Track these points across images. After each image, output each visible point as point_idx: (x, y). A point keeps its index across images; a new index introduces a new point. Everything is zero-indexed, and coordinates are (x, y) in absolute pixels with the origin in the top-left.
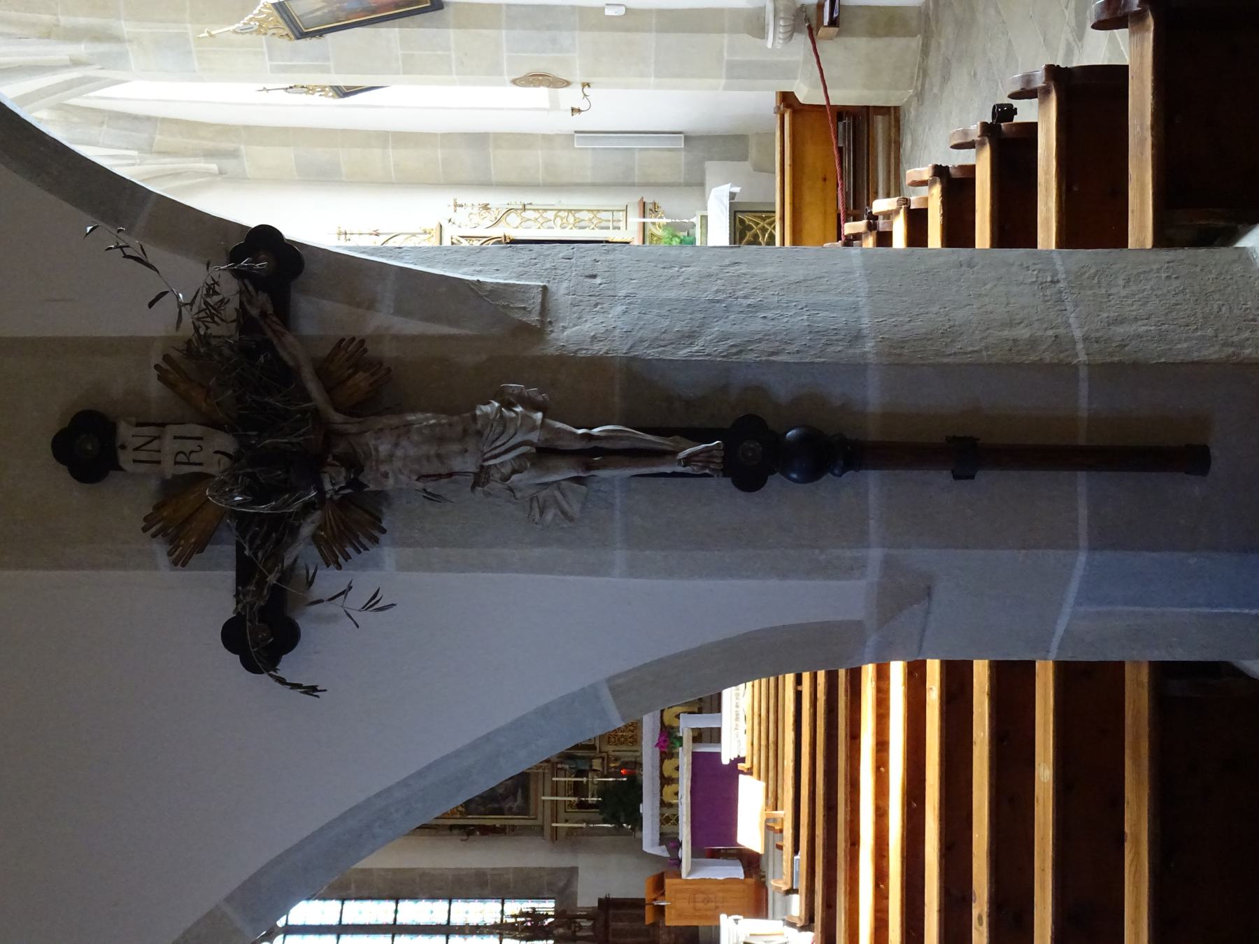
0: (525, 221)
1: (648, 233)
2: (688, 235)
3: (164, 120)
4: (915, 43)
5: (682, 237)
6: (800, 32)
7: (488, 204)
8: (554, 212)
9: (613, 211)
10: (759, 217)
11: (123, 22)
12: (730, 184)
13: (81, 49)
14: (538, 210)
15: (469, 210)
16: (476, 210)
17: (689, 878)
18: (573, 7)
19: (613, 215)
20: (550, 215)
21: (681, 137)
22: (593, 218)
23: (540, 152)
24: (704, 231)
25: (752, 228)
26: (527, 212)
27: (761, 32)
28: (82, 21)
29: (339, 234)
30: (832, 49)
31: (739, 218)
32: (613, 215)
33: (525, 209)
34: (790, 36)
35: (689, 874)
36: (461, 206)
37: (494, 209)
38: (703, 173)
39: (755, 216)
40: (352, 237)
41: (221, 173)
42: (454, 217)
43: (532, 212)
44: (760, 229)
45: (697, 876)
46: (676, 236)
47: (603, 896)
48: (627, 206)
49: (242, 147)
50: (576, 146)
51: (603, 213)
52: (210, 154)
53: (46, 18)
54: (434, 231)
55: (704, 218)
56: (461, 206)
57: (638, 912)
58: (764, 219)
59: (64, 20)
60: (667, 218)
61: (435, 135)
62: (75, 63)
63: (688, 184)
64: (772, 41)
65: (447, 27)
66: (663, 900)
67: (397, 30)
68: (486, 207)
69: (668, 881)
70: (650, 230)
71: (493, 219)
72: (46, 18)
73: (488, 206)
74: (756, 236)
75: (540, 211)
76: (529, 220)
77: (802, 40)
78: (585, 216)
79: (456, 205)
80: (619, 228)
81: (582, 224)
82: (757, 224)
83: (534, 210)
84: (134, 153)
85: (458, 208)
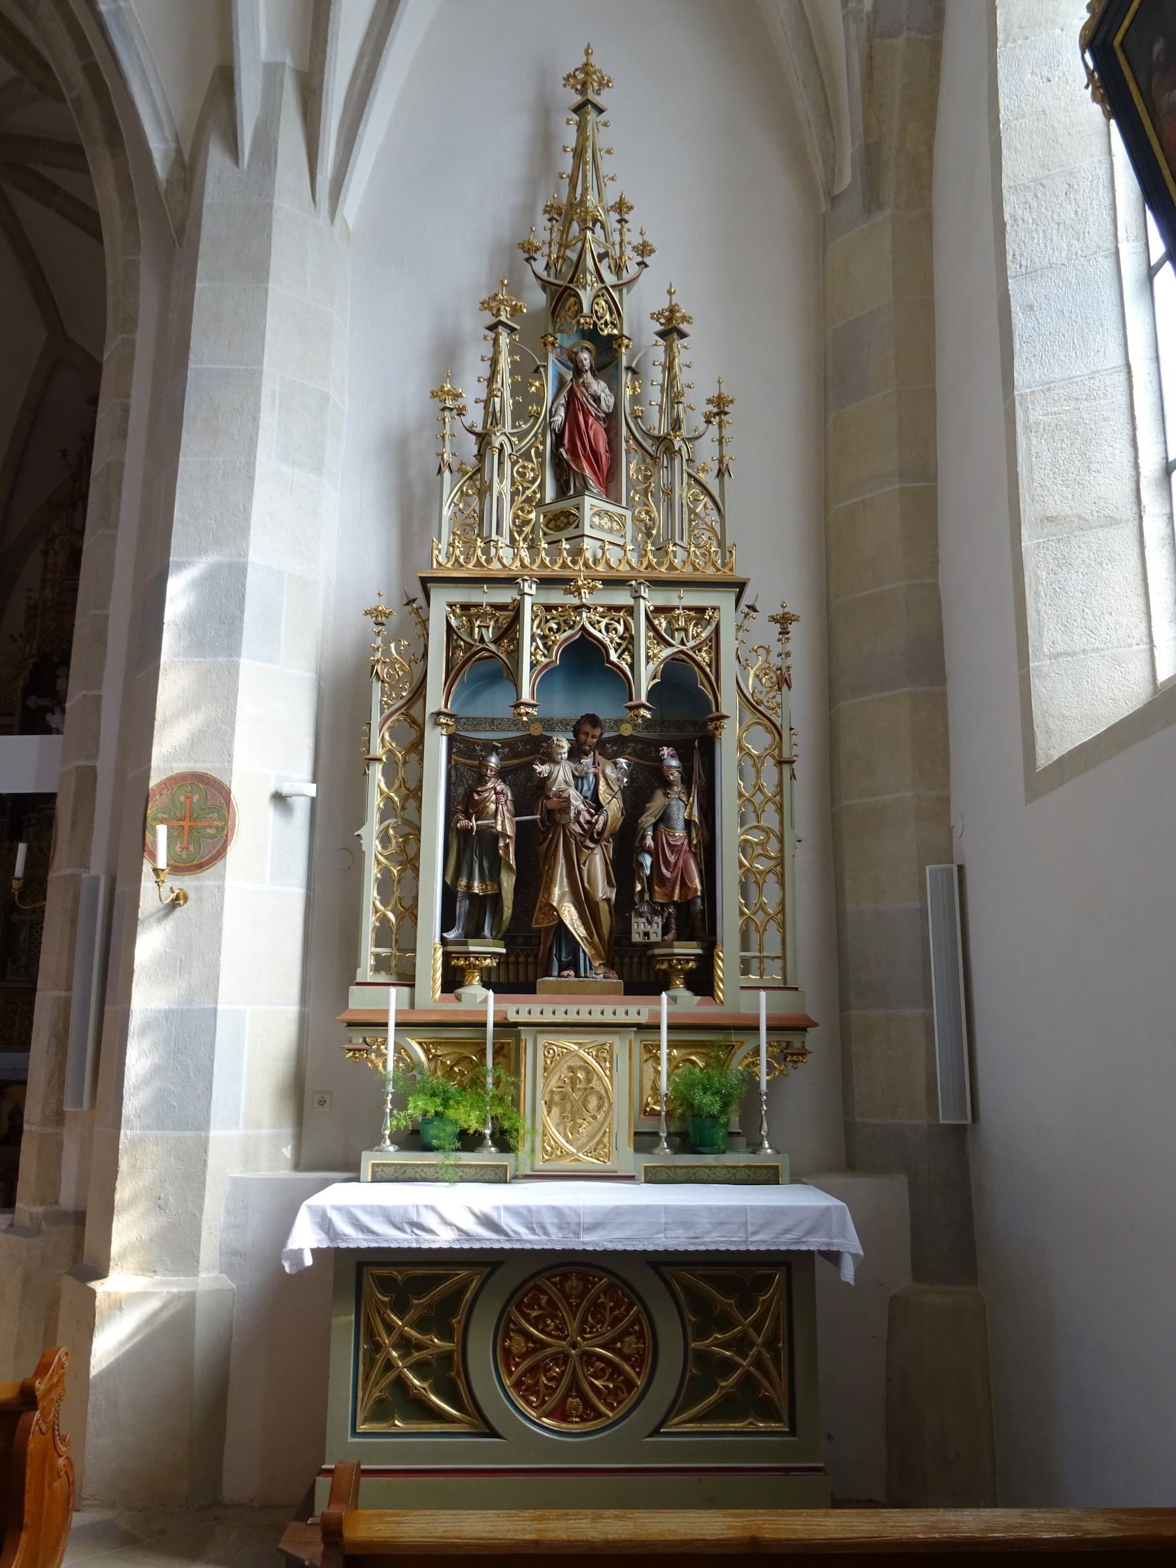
0: (755, 765)
1: (734, 1038)
2: (731, 1134)
3: (936, 48)
5: (723, 1120)
7: (789, 687)
8: (776, 828)
9: (783, 958)
10: (775, 1331)
12: (861, 1252)
14: (780, 792)
15: (777, 648)
16: (776, 661)
19: (773, 958)
20: (770, 819)
21: (966, 1119)
22: (767, 914)
23: (909, 793)
24: (741, 1175)
25: (746, 1312)
26: (775, 770)
31: (772, 1277)
32: (773, 958)
33: (780, 763)
36: (784, 632)
37: (778, 699)
38: (875, 1169)
39: (780, 1376)
40: (713, 430)
43: (776, 781)
44: (745, 1334)
46: (725, 1105)
48: (796, 989)
49: (888, 212)
50: (928, 868)
51: (779, 936)
54: (730, 573)
55: (768, 1176)
56: (784, 632)
57: (637, 1130)
58: (770, 1344)
61: (935, 574)
63: (849, 1130)
68: (783, 681)
70: (742, 1043)
71: (758, 696)
73: (785, 687)
74: (726, 1323)
75: (778, 798)
76: (758, 772)
78: (770, 898)
80: (745, 971)
81: (753, 889)
82: (758, 1325)
83: (780, 784)
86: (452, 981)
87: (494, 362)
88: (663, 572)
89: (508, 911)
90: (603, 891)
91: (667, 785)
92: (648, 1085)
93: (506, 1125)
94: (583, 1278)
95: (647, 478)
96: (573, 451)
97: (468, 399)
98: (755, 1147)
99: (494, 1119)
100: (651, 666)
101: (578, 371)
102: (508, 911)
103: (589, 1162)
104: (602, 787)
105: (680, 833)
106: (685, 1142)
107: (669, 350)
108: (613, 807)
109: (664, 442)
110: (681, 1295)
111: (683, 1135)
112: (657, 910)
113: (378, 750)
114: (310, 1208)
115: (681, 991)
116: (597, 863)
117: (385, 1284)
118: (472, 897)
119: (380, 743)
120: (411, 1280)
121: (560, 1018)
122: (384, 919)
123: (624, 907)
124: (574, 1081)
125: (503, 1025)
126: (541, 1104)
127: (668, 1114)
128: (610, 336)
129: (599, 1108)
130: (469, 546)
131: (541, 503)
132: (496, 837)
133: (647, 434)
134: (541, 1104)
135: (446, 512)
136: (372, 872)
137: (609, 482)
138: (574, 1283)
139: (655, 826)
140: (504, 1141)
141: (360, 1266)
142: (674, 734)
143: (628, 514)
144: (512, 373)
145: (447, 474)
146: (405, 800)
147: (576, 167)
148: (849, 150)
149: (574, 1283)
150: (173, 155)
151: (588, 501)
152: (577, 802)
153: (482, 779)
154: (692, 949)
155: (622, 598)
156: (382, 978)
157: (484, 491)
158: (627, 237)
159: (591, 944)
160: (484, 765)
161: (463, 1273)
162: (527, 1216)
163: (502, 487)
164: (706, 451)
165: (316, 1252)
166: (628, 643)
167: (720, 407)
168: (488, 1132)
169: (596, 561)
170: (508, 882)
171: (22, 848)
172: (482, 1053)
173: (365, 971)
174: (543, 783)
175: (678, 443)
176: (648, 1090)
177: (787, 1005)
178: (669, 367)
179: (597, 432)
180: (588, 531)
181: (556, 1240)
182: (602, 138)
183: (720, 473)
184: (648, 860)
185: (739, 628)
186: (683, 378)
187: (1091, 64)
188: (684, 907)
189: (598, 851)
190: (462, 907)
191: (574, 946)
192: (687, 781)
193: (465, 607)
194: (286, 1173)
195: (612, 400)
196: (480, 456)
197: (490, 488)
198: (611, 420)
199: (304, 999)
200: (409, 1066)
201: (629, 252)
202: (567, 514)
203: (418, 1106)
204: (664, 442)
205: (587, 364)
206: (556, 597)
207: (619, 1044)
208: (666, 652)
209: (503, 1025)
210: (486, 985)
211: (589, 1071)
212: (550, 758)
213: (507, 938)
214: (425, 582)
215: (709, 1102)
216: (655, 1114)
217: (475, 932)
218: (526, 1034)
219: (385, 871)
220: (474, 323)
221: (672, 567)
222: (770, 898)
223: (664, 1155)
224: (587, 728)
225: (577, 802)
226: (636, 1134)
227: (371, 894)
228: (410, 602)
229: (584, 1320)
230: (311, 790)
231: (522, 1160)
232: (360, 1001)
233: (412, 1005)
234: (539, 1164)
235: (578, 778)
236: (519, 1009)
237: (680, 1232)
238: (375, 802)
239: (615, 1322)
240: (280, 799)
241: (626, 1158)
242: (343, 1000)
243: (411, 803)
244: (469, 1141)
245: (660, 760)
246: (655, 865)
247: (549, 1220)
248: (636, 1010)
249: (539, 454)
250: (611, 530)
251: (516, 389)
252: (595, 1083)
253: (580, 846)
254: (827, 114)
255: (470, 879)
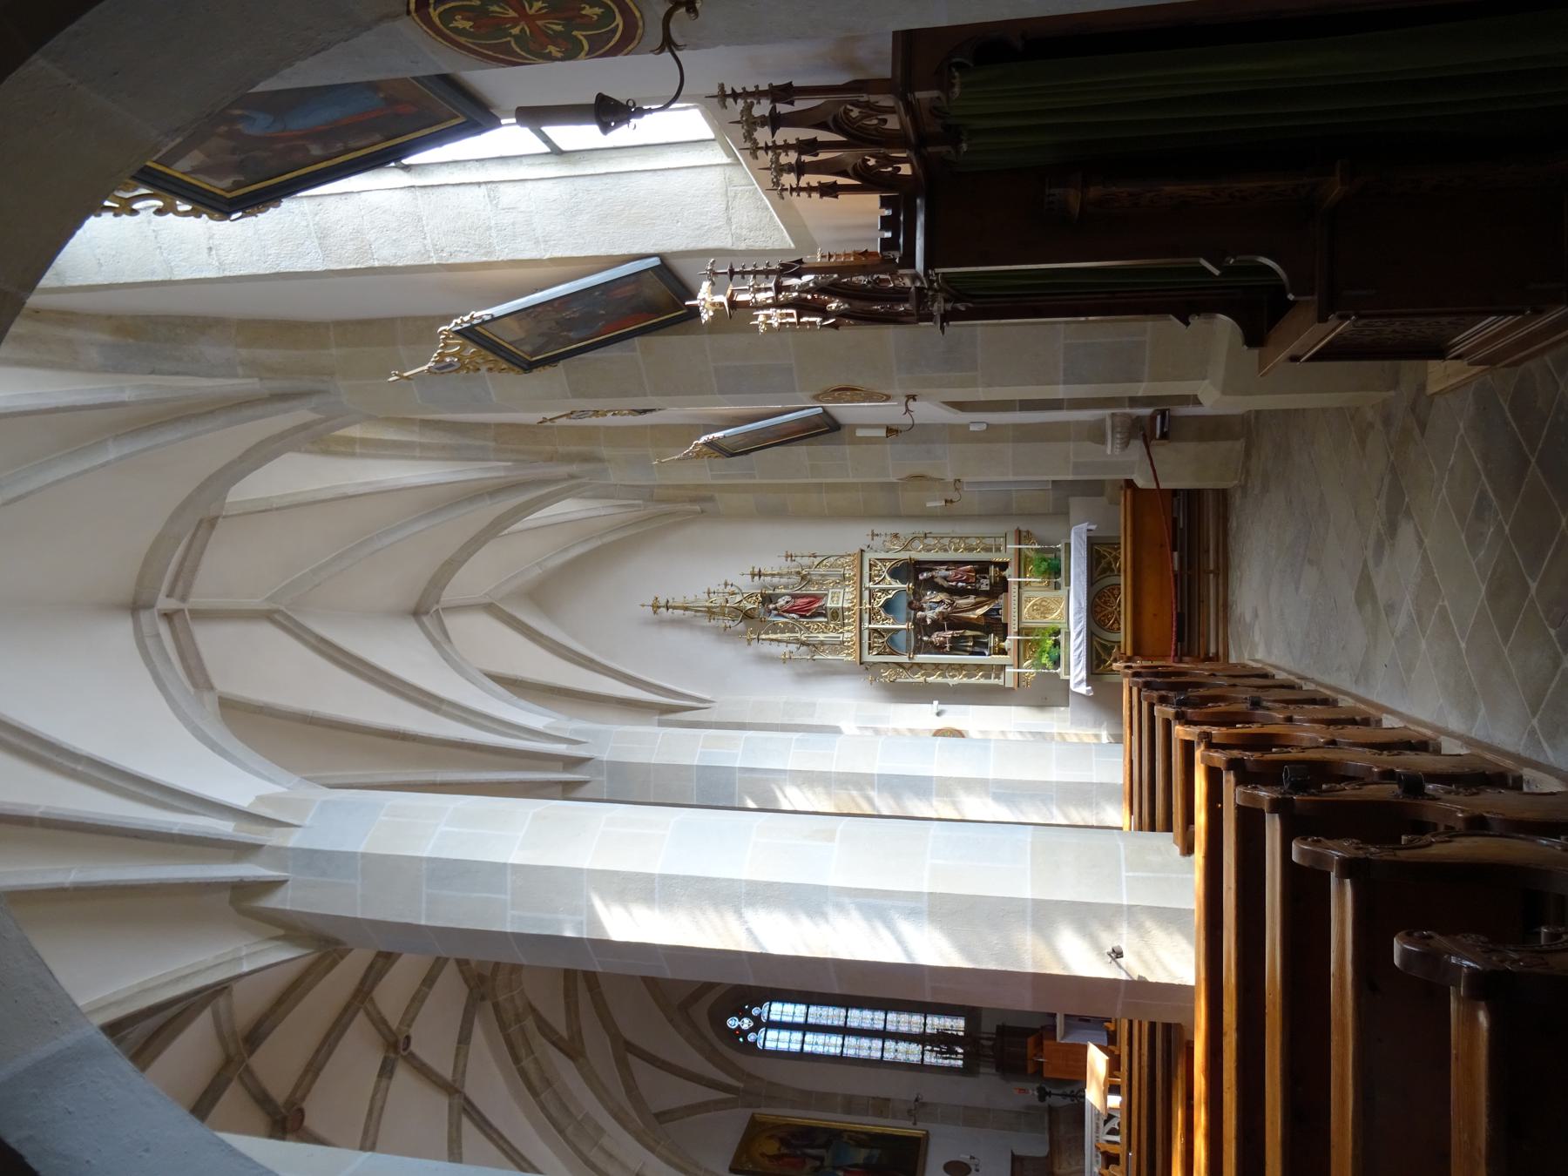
1: (1023, 557)
4: (1239, 445)
6: (1136, 438)
9: (995, 537)
11: (603, 448)
13: (574, 468)
14: (936, 537)
15: (883, 538)
16: (888, 538)
17: (1062, 1042)
18: (944, 425)
20: (946, 541)
27: (1101, 439)
28: (574, 449)
29: (787, 557)
30: (1161, 451)
33: (926, 537)
34: (1126, 444)
35: (1062, 1039)
36: (877, 535)
38: (1068, 507)
40: (798, 559)
41: (702, 512)
42: (872, 543)
45: (1067, 1041)
46: (1045, 560)
47: (1000, 1024)
50: (965, 489)
52: (693, 500)
53: (548, 448)
55: (1068, 545)
56: (877, 535)
59: (561, 449)
60: (1039, 544)
62: (572, 477)
64: (1110, 449)
65: (845, 444)
66: (1041, 1057)
67: (804, 447)
69: (1046, 1042)
72: (548, 448)
74: (1110, 563)
77: (1137, 446)
79: (873, 535)
82: (1110, 553)
83: (933, 537)
84: (640, 502)
85: (875, 538)
86: (1003, 652)
87: (772, 640)
88: (857, 578)
89: (978, 633)
90: (972, 600)
91: (933, 577)
92: (1039, 585)
93: (1051, 632)
94: (1096, 606)
95: (817, 584)
96: (808, 611)
97: (787, 650)
98: (1059, 550)
99: (1050, 636)
100: (893, 583)
101: (776, 609)
102: (978, 633)
103: (1063, 605)
104: (934, 600)
105: (950, 573)
106: (1057, 573)
107: (766, 575)
108: (941, 596)
109: (803, 578)
110: (1102, 576)
111: (1056, 573)
112: (977, 580)
113: (922, 679)
114: (1075, 687)
115: (1006, 573)
116: (961, 602)
117: (1098, 666)
118: (974, 646)
119: (919, 678)
120: (1097, 658)
121: (1016, 614)
122: (982, 676)
123: (977, 592)
124: (1037, 610)
125: (1019, 633)
126: (1045, 620)
127: (1049, 578)
128: (761, 596)
129: (1045, 601)
130: (848, 648)
131: (827, 623)
132: (953, 637)
133: (800, 584)
134: (1045, 620)
135: (830, 657)
136: (965, 680)
137: (817, 598)
138: (1098, 609)
139: (948, 581)
140: (1057, 633)
141: (1092, 674)
142: (912, 574)
143: (831, 591)
144: (776, 633)
145: (815, 657)
146: (939, 670)
147: (692, 610)
148: (688, 507)
149: (1098, 609)
150: (279, 943)
151: (828, 605)
152: (940, 609)
153: (932, 643)
154: (992, 568)
155: (866, 594)
156: (1002, 676)
157: (822, 643)
158: (721, 591)
159: (990, 604)
160: (927, 643)
161: (1095, 643)
162: (1077, 622)
163: (821, 637)
164: (806, 561)
165: (1088, 686)
166: (885, 591)
167: (789, 556)
168: (1054, 638)
169: (852, 602)
170: (969, 633)
171: (1217, 272)
172: (1028, 641)
173: (1000, 682)
174: (934, 621)
175: (804, 572)
176: (1041, 585)
177: (1012, 538)
178: (773, 575)
179: (800, 601)
180: (840, 605)
181: (1084, 614)
182: (679, 601)
183: (815, 557)
184: (960, 584)
185: (876, 551)
186: (785, 571)
187: (240, 214)
188: (977, 571)
189: (957, 602)
190: (977, 649)
191: (991, 610)
192: (931, 570)
193: (869, 649)
194: (1069, 709)
195: (787, 597)
196: (808, 645)
197: (822, 641)
198: (794, 597)
199: (1010, 705)
200: (1032, 665)
201: (726, 590)
202: (833, 613)
203: (1044, 660)
204: (803, 578)
205: (774, 606)
206: (866, 617)
207: (1025, 595)
208: (888, 578)
209: (1019, 633)
210: (1004, 641)
211: (1034, 605)
212: (924, 619)
213: (988, 633)
214: (861, 663)
215: (1044, 565)
216: (1049, 582)
217: (986, 645)
218: (1022, 626)
219: (965, 676)
220: (751, 650)
221: (855, 575)
222: (974, 542)
223: (1061, 580)
224: (913, 606)
225: (940, 609)
226: (1055, 589)
227: (973, 680)
228: (867, 669)
229: (1109, 606)
230: (936, 703)
231: (1062, 626)
232: (1010, 683)
233: (1011, 665)
234: (1064, 621)
235: (931, 609)
236: (1013, 628)
237: (1081, 577)
238: (940, 680)
239: (1109, 597)
240: (938, 714)
241: (1062, 593)
242: (1012, 689)
243: (940, 667)
244: (1057, 644)
245: (925, 580)
246: (962, 581)
247: (1078, 617)
248: (1013, 589)
249: (808, 623)
250: (838, 597)
251: (783, 632)
252: (1038, 603)
253: (956, 608)
254: (671, 514)
255: (967, 646)
